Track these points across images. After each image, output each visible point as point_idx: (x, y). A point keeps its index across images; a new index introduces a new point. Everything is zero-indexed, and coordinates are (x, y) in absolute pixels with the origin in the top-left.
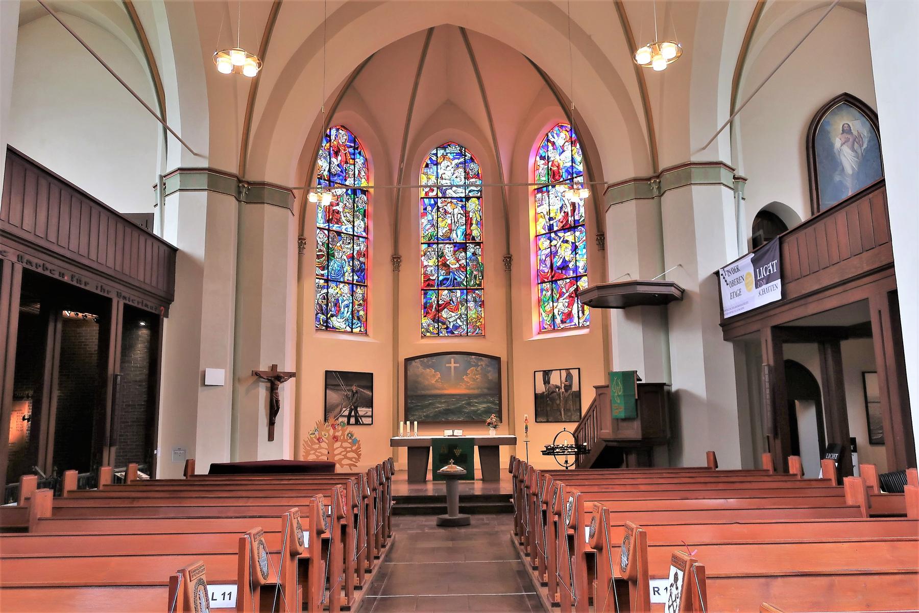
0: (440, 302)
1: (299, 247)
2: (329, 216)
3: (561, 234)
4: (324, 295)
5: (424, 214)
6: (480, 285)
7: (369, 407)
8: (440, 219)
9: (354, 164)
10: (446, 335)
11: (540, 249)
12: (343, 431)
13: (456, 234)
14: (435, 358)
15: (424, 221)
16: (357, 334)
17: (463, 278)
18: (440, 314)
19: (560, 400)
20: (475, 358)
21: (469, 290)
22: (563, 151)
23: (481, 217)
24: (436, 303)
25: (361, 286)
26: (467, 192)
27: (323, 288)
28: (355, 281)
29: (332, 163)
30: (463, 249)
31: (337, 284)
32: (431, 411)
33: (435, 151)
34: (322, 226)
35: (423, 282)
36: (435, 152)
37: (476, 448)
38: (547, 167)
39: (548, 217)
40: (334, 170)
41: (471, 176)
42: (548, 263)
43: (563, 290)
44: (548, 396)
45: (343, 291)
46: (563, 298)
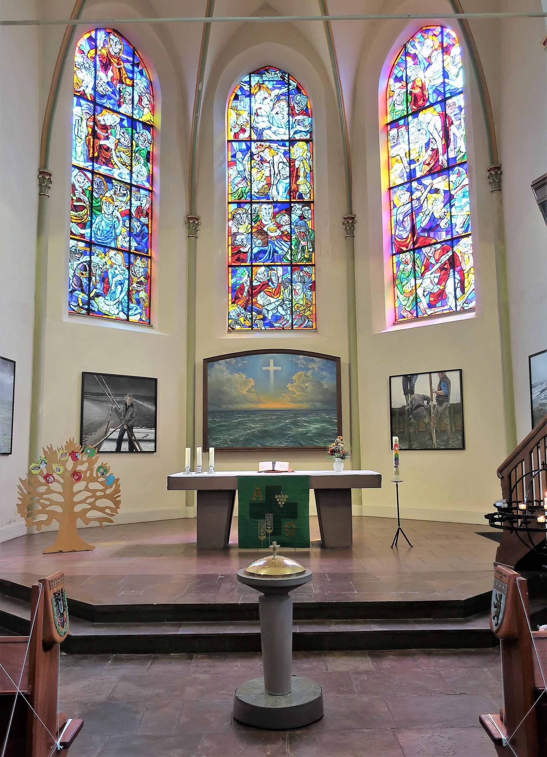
0: (255, 283)
1: (40, 185)
2: (93, 153)
3: (427, 181)
4: (85, 264)
5: (232, 164)
6: (309, 260)
7: (151, 428)
8: (254, 171)
9: (133, 86)
10: (263, 328)
11: (395, 206)
12: (91, 463)
13: (277, 190)
14: (247, 358)
15: (232, 172)
16: (134, 323)
17: (286, 250)
18: (254, 300)
19: (430, 418)
20: (303, 359)
21: (294, 267)
22: (430, 64)
23: (310, 168)
24: (249, 284)
25: (142, 256)
26: (292, 133)
27: (84, 253)
28: (133, 248)
29: (99, 79)
30: (286, 210)
31: (105, 250)
32: (240, 434)
33: (247, 79)
34: (82, 165)
35: (230, 255)
36: (248, 80)
37: (312, 492)
38: (405, 90)
39: (408, 159)
40: (101, 89)
41: (297, 112)
42: (408, 224)
43: (430, 261)
44: (411, 411)
45: (114, 261)
46: (430, 272)
